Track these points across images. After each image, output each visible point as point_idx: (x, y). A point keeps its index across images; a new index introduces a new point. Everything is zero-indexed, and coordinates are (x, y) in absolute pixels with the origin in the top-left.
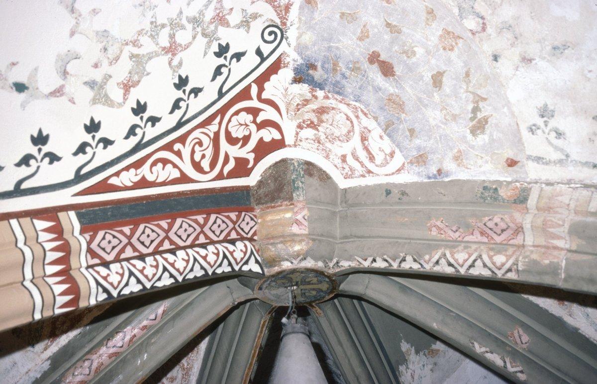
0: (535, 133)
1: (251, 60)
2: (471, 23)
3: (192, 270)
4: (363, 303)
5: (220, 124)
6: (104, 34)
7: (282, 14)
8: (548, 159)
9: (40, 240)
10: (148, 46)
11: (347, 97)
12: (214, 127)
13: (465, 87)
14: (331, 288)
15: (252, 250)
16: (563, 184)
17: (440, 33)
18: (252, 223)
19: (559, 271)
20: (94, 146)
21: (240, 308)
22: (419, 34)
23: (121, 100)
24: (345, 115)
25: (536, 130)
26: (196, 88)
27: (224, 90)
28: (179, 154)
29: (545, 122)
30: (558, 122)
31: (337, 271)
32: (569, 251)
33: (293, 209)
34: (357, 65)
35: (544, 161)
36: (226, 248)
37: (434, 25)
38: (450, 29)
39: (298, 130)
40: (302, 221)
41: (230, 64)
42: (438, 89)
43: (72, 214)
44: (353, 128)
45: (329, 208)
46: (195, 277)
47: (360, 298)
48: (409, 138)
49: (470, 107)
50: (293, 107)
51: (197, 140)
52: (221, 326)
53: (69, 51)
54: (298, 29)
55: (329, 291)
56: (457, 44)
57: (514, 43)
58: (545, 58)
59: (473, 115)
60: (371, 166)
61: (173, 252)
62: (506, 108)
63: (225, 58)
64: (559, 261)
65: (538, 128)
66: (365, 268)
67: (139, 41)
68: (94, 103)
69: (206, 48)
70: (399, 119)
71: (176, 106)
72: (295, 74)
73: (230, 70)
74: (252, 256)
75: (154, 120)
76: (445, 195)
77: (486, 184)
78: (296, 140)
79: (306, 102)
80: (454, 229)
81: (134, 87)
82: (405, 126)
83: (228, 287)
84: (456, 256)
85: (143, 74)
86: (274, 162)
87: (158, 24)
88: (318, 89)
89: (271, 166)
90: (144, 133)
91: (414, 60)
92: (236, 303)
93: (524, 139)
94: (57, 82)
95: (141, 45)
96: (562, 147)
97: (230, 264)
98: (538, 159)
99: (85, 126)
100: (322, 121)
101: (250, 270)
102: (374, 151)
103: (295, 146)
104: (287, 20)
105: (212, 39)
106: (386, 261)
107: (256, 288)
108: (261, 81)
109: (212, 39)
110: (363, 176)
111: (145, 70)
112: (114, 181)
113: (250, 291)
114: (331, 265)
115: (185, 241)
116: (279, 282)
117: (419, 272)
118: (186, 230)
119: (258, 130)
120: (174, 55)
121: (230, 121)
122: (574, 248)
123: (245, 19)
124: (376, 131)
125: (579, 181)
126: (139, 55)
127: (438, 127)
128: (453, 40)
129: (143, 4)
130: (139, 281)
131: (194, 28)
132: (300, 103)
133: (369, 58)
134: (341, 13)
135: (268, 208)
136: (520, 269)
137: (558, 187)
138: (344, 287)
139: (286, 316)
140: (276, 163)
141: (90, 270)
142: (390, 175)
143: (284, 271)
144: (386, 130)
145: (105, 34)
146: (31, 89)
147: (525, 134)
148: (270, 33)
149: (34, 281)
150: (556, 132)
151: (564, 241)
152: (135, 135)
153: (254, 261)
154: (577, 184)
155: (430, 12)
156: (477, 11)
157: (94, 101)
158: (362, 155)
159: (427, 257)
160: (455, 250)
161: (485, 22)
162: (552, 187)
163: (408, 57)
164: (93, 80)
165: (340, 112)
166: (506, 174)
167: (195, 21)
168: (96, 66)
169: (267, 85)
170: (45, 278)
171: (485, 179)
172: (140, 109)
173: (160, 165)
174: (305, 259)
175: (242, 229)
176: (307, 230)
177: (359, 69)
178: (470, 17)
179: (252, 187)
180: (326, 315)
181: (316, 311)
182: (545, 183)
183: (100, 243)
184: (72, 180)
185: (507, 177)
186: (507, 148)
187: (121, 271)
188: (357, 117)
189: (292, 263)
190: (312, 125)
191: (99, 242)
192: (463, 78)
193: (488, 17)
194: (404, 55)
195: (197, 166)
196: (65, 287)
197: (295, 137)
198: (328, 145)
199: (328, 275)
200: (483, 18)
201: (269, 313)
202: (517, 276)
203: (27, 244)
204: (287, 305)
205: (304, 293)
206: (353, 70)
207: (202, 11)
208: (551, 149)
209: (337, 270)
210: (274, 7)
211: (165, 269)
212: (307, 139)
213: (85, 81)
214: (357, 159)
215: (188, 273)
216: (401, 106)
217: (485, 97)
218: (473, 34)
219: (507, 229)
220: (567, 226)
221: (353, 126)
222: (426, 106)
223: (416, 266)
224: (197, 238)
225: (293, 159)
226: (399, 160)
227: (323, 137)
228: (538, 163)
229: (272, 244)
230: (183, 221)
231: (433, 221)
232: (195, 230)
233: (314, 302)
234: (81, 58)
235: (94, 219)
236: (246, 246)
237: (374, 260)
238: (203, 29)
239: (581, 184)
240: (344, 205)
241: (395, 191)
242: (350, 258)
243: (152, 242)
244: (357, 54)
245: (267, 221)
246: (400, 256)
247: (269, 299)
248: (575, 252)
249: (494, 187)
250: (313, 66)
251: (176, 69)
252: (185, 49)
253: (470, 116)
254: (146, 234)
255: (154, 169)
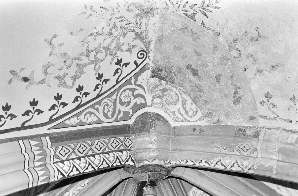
0: (263, 105)
1: (132, 66)
2: (234, 53)
3: (102, 164)
4: (182, 181)
5: (117, 95)
6: (65, 55)
7: (147, 46)
8: (269, 117)
9: (32, 150)
10: (85, 60)
11: (176, 84)
12: (114, 98)
13: (231, 82)
14: (167, 173)
15: (130, 154)
16: (275, 129)
17: (220, 57)
18: (130, 142)
19: (273, 170)
20: (58, 106)
21: (123, 182)
22: (210, 57)
23: (71, 85)
24: (175, 92)
25: (263, 104)
26: (106, 79)
27: (119, 80)
28: (97, 110)
29: (268, 100)
30: (274, 100)
31: (169, 166)
32: (278, 161)
33: (150, 136)
34: (181, 70)
35: (267, 118)
36: (118, 154)
37: (217, 53)
38: (224, 55)
39: (153, 99)
40: (154, 142)
41: (122, 68)
42: (218, 82)
43: (47, 138)
44: (179, 99)
45: (166, 136)
46: (104, 167)
47: (180, 179)
48: (205, 104)
49: (233, 91)
50: (151, 88)
51: (106, 103)
52: (114, 190)
53: (48, 63)
54: (154, 52)
55: (166, 175)
56: (227, 62)
57: (254, 63)
58: (268, 70)
59: (234, 95)
60: (186, 117)
61: (93, 156)
62: (250, 93)
63: (120, 65)
64: (273, 165)
65: (265, 103)
66: (183, 165)
67: (81, 58)
68: (59, 86)
69: (111, 61)
70: (200, 95)
71: (97, 87)
72: (152, 73)
73: (122, 71)
74: (130, 158)
75: (86, 94)
76: (221, 132)
77: (240, 128)
78: (152, 104)
79: (157, 86)
80: (225, 148)
81: (78, 79)
82: (203, 99)
83: (118, 172)
84: (225, 161)
85: (82, 73)
86: (141, 113)
87: (89, 50)
88: (163, 80)
89: (140, 115)
90: (82, 100)
91: (208, 68)
92: (122, 179)
93: (258, 107)
94: (43, 77)
95: (82, 60)
96: (276, 112)
97: (120, 162)
98: (264, 117)
99: (55, 97)
100: (164, 95)
101: (129, 164)
102: (188, 109)
103: (151, 106)
104: (149, 48)
105: (114, 57)
106: (193, 162)
107: (132, 172)
108: (137, 76)
109: (114, 57)
110: (183, 121)
111: (83, 71)
112: (67, 122)
113: (128, 174)
114: (167, 163)
115: (99, 151)
116: (143, 170)
117: (208, 167)
118: (100, 146)
119: (134, 99)
120: (96, 64)
121: (121, 94)
122: (280, 159)
123: (129, 48)
124: (189, 101)
125: (283, 128)
126: (80, 64)
127: (218, 100)
128: (226, 60)
129: (83, 41)
130: (77, 170)
131: (106, 52)
132: (154, 86)
133: (187, 67)
134: (174, 46)
135: (138, 135)
136: (255, 168)
137: (273, 130)
138: (173, 173)
139: (146, 186)
140: (143, 114)
141: (55, 164)
142: (195, 121)
143: (145, 165)
144: (194, 100)
145: (65, 55)
146: (30, 80)
147: (259, 105)
148: (141, 54)
149: (29, 169)
150: (273, 105)
151: (276, 156)
152: (78, 101)
153: (131, 160)
154: (282, 129)
155: (216, 47)
156: (237, 48)
157: (59, 86)
158: (182, 111)
159: (212, 161)
160: (225, 158)
161: (240, 53)
162: (271, 130)
163: (205, 67)
164: (59, 76)
165: (173, 91)
166: (249, 124)
167: (107, 49)
168: (60, 69)
169: (139, 78)
170: (34, 168)
171: (240, 125)
172: (80, 89)
173: (88, 115)
174: (155, 160)
175: (126, 145)
176: (156, 146)
177: (182, 71)
178: (234, 50)
179: (131, 125)
180: (164, 186)
181: (159, 184)
182: (267, 128)
183: (60, 151)
184: (48, 122)
185: (250, 125)
186: (250, 111)
187: (69, 165)
188: (181, 94)
189: (149, 161)
190: (159, 97)
191: (59, 151)
192: (230, 78)
193: (242, 51)
194: (203, 66)
195: (106, 115)
196: (43, 172)
197: (151, 102)
198: (167, 106)
199: (166, 167)
200: (239, 51)
201: (137, 184)
202: (254, 171)
203: (26, 152)
204: (146, 181)
205: (154, 176)
206: (179, 72)
207: (110, 44)
208: (270, 113)
209: (170, 165)
210: (143, 42)
211: (90, 164)
212: (157, 103)
213: (55, 76)
214: (180, 113)
215: (100, 166)
216: (201, 90)
217: (240, 87)
218: (235, 58)
219: (249, 149)
220: (277, 149)
221: (179, 98)
222: (213, 90)
223: (207, 165)
224: (105, 149)
225: (150, 112)
226: (199, 114)
227: (164, 102)
228: (264, 119)
229: (140, 152)
230: (98, 141)
231: (215, 144)
232: (104, 145)
233: (158, 179)
234: (54, 66)
235: (56, 139)
236: (127, 153)
237: (187, 161)
238: (110, 52)
239: (284, 130)
240: (174, 134)
241: (197, 129)
242: (176, 160)
243: (84, 151)
244: (181, 65)
245: (137, 142)
246: (199, 160)
247: (138, 178)
248: (281, 161)
249: (244, 129)
250: (161, 70)
251: (97, 71)
252: (102, 61)
253: (233, 96)
254: (81, 147)
255: (86, 117)
